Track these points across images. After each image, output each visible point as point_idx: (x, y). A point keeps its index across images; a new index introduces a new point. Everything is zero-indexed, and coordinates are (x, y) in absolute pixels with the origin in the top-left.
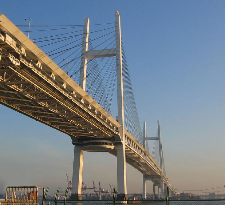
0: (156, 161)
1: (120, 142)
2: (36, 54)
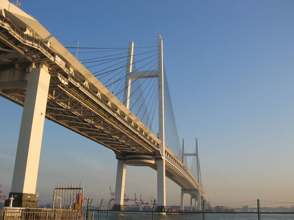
0: (194, 176)
1: (160, 157)
2: (83, 74)
